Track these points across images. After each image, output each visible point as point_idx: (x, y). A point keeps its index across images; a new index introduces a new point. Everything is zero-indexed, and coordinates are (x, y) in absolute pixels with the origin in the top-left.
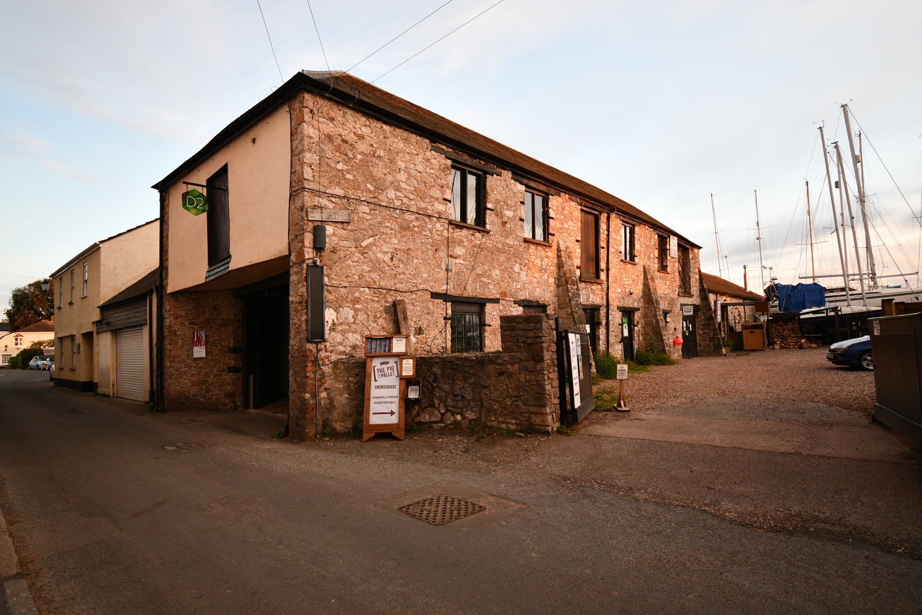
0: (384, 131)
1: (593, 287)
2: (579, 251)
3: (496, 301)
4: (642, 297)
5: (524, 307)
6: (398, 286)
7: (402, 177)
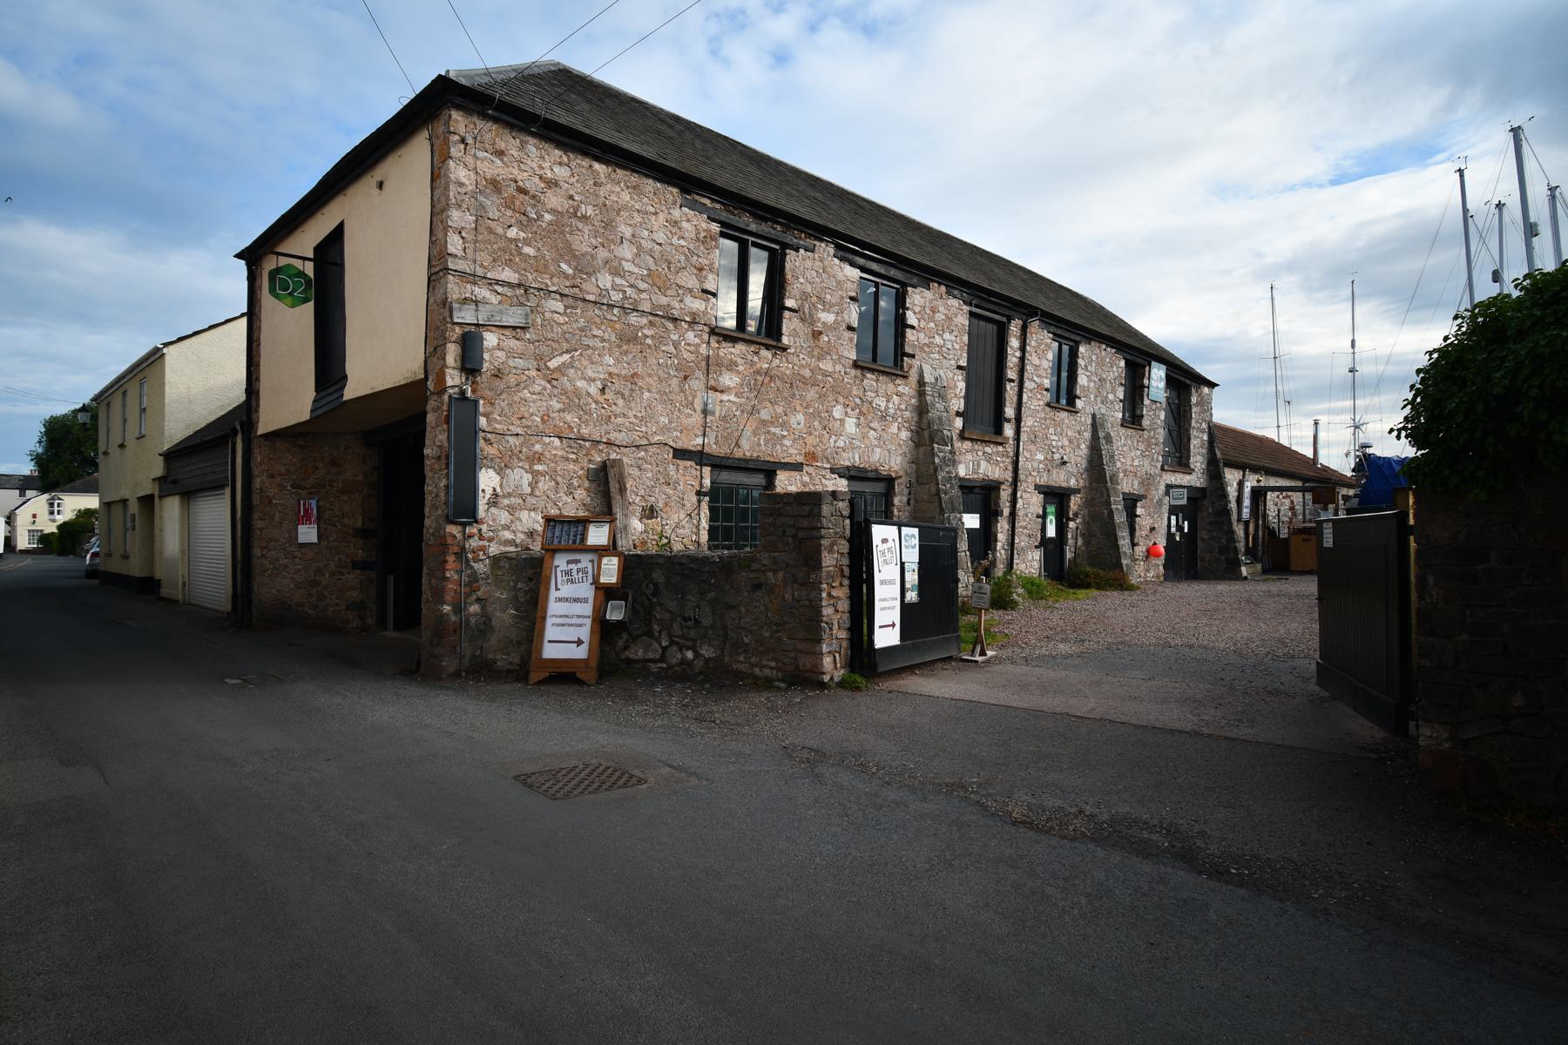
0: (595, 174)
1: (988, 449)
2: (962, 385)
3: (797, 467)
4: (1087, 469)
5: (850, 478)
6: (613, 436)
7: (627, 251)
